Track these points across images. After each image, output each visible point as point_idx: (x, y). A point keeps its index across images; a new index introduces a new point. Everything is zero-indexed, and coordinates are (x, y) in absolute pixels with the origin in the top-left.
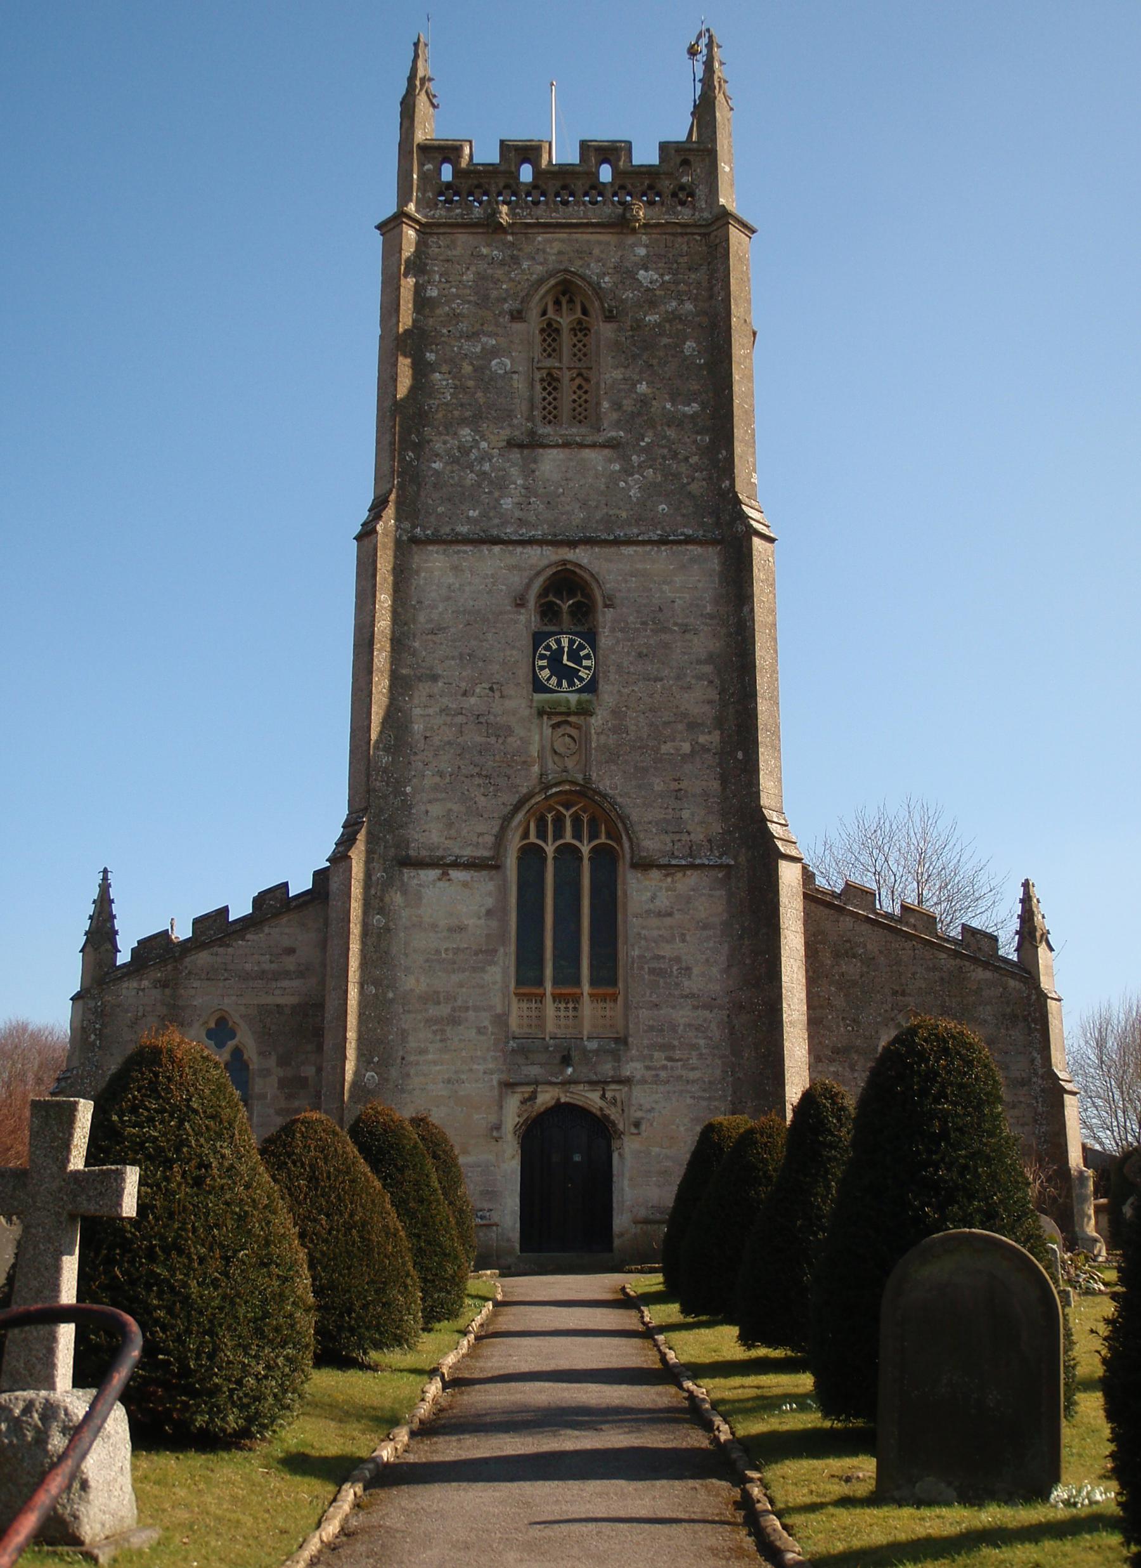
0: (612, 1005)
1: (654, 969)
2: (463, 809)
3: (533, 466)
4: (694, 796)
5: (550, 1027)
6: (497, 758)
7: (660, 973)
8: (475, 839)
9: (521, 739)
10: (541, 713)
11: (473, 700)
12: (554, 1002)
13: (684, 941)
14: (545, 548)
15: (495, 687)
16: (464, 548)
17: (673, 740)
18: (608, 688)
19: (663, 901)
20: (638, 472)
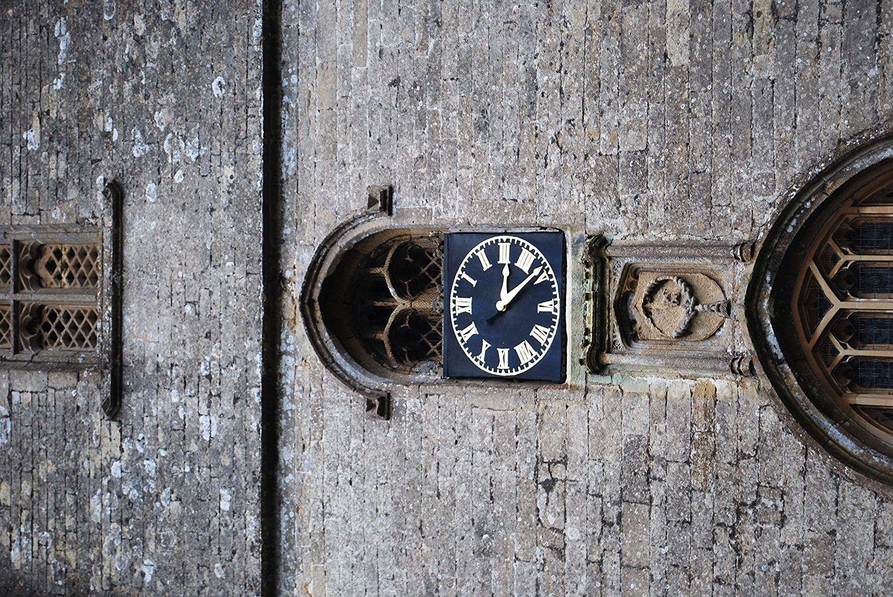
3: (149, 368)
6: (696, 483)
10: (596, 366)
11: (572, 533)
14: (284, 347)
16: (283, 524)
17: (661, 34)
18: (548, 201)
20: (160, 144)
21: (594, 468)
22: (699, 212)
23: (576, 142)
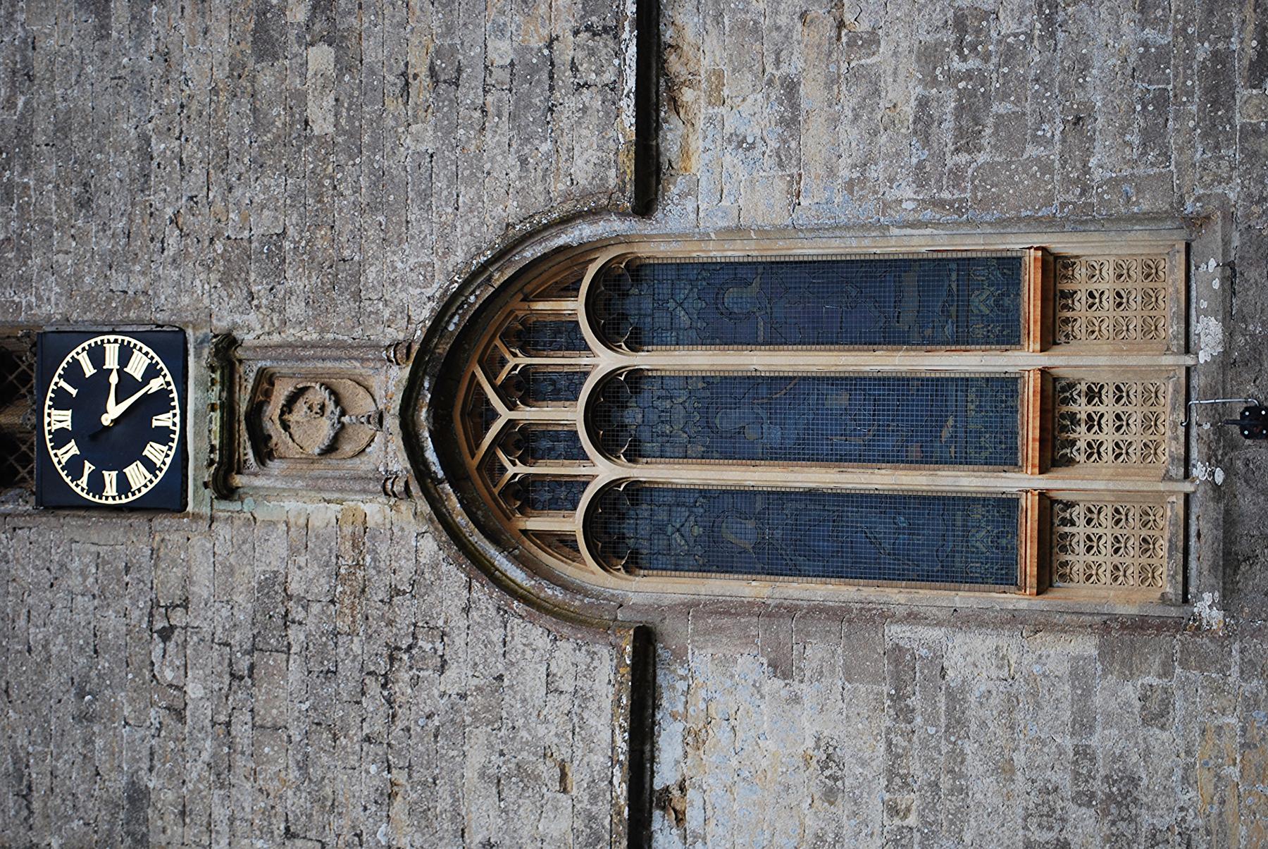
0: (1081, 272)
1: (960, 132)
2: (480, 734)
4: (449, 30)
5: (1142, 481)
6: (342, 625)
7: (971, 108)
8: (565, 702)
9: (293, 551)
10: (224, 489)
11: (194, 690)
12: (1070, 462)
13: (872, 41)
15: (158, 626)
17: (301, 97)
18: (165, 294)
19: (752, 112)
21: (220, 613)
22: (346, 306)
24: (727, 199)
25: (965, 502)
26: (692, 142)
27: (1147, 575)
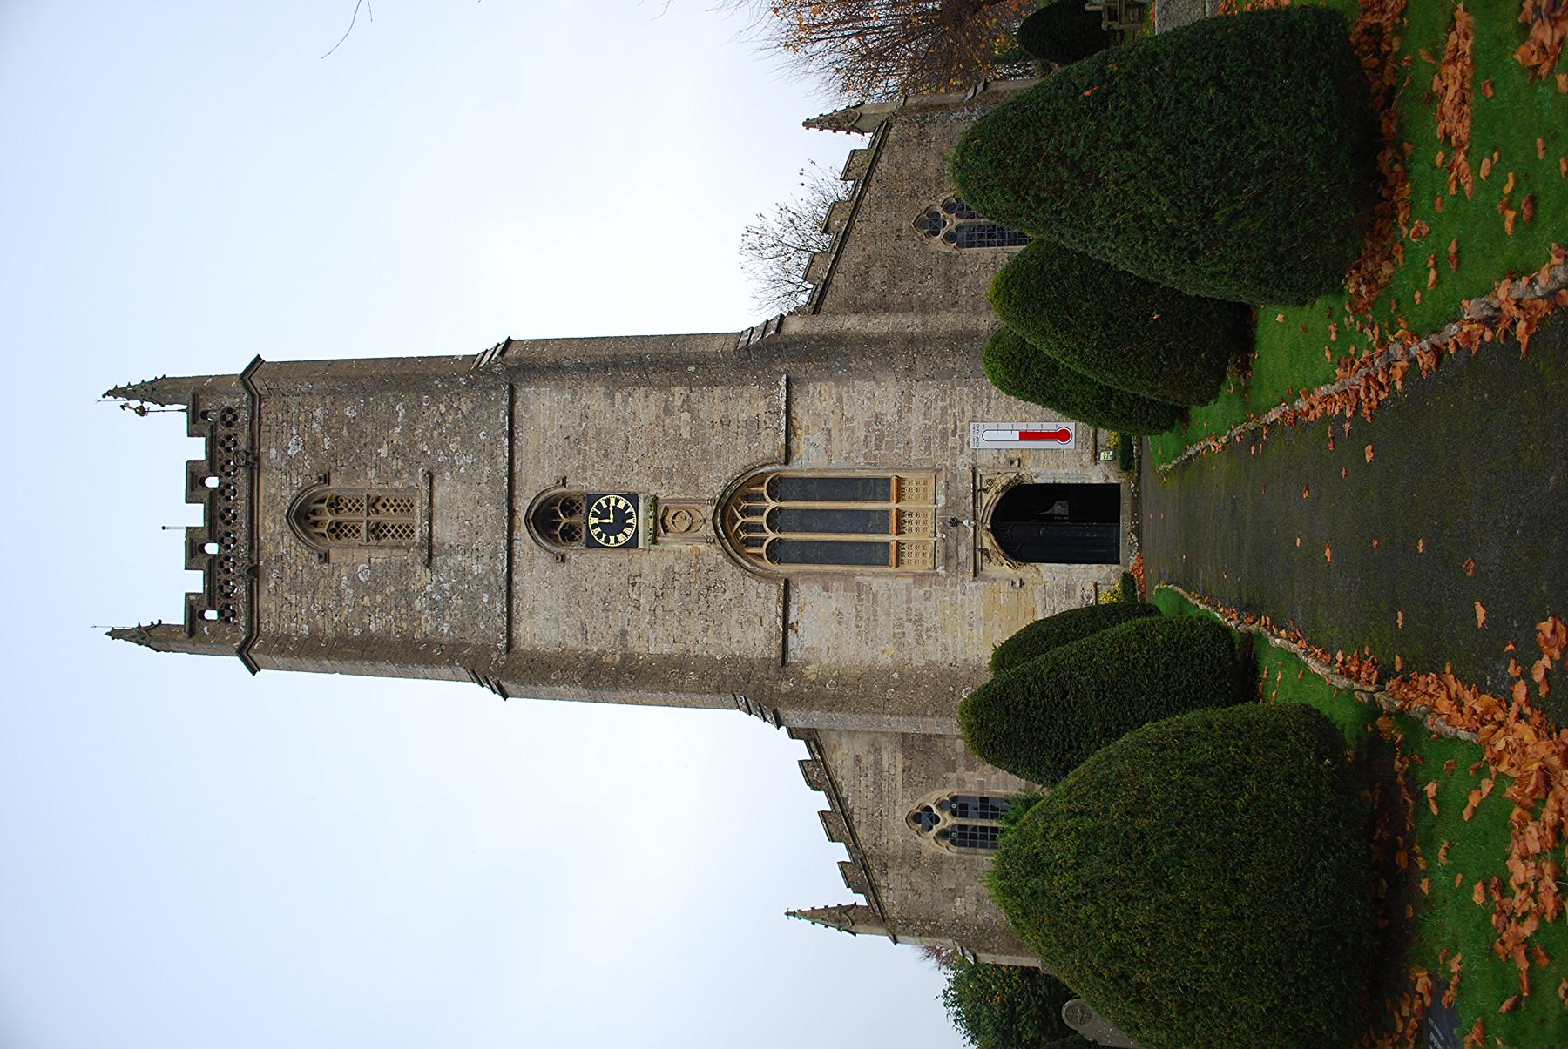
7: (879, 439)
11: (643, 601)
19: (818, 437)
21: (653, 577)
22: (694, 488)
23: (646, 463)
24: (810, 460)
25: (876, 544)
26: (801, 445)
27: (924, 562)
